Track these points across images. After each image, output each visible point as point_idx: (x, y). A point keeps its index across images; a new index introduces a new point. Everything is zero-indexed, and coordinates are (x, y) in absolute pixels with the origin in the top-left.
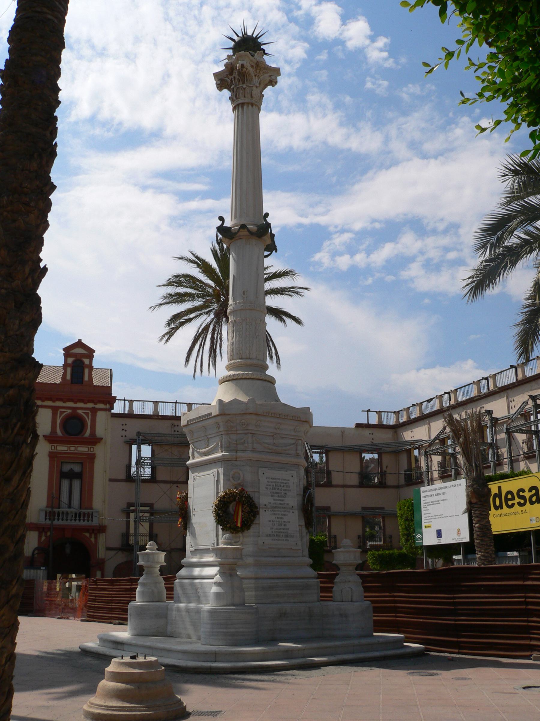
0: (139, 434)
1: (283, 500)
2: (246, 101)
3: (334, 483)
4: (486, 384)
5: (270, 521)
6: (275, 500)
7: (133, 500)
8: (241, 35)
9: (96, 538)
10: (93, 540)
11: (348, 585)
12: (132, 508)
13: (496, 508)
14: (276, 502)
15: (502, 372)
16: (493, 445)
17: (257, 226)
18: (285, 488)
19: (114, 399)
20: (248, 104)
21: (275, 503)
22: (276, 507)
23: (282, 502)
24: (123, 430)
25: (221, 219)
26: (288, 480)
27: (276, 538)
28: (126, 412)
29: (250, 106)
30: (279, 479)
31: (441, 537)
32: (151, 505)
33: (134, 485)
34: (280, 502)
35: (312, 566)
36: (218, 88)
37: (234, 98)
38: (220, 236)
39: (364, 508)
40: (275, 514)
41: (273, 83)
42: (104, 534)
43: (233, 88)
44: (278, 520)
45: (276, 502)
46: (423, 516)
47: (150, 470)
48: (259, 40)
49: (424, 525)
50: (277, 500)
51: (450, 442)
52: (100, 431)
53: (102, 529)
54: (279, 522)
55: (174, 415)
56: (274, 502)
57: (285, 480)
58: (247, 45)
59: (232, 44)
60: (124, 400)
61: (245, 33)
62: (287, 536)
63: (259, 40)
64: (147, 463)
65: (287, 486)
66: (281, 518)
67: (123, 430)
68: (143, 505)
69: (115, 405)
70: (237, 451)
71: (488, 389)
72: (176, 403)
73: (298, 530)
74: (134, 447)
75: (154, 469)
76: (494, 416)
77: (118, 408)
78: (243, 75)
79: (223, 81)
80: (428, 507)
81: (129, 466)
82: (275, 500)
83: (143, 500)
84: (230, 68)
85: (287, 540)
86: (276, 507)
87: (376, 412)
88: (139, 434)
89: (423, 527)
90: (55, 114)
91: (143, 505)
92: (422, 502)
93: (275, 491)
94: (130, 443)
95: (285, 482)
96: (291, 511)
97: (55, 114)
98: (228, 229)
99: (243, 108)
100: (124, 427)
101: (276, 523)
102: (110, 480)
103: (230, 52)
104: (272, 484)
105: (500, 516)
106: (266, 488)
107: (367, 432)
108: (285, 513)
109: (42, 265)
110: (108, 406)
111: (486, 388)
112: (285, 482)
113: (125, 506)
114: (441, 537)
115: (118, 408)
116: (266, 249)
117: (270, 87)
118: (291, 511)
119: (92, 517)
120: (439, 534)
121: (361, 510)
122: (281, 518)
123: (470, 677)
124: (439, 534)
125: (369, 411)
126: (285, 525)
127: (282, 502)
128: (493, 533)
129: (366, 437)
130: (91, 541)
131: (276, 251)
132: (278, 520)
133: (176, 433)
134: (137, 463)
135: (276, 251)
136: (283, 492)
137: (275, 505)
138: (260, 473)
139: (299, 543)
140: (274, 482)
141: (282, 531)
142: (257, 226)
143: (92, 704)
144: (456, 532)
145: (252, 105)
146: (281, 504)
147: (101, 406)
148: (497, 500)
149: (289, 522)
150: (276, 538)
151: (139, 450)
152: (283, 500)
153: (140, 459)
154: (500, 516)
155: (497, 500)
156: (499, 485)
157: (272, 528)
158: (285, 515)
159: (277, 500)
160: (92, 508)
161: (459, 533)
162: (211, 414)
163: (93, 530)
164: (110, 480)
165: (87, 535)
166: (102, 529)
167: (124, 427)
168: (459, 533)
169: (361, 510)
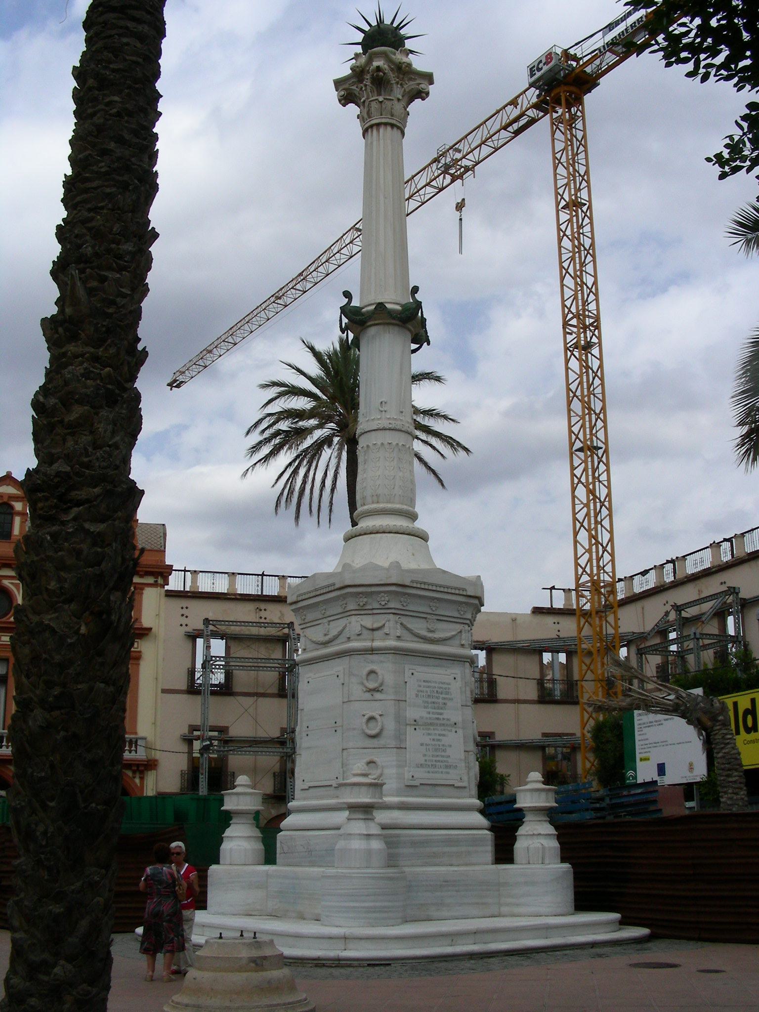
0: (207, 621)
1: (441, 714)
2: (384, 121)
3: (501, 695)
4: (729, 549)
5: (422, 745)
6: (429, 713)
7: (198, 722)
8: (374, 23)
9: (142, 779)
10: (137, 781)
11: (537, 839)
12: (196, 733)
13: (748, 730)
14: (431, 716)
15: (753, 530)
16: (740, 639)
17: (402, 306)
18: (444, 696)
19: (170, 569)
20: (386, 124)
21: (430, 718)
22: (431, 724)
23: (441, 717)
24: (183, 615)
25: (347, 295)
26: (449, 684)
27: (432, 770)
28: (187, 589)
29: (389, 128)
30: (436, 682)
31: (664, 775)
32: (223, 730)
33: (198, 699)
34: (437, 716)
35: (482, 812)
36: (340, 101)
37: (366, 116)
38: (345, 320)
39: (545, 735)
40: (429, 734)
41: (422, 95)
42: (154, 772)
43: (364, 102)
44: (433, 743)
45: (431, 716)
46: (637, 743)
47: (223, 676)
48: (402, 32)
49: (638, 756)
50: (433, 713)
51: (673, 636)
52: (147, 620)
53: (150, 765)
54: (435, 745)
55: (260, 593)
56: (428, 716)
57: (444, 683)
58: (383, 38)
59: (360, 37)
60: (185, 571)
61: (380, 21)
62: (447, 767)
63: (402, 32)
64: (219, 665)
65: (447, 693)
66: (439, 740)
67: (183, 615)
68: (212, 729)
69: (171, 578)
70: (373, 640)
71: (733, 556)
72: (263, 575)
73: (463, 758)
74: (200, 642)
75: (228, 675)
76: (741, 595)
77: (175, 583)
78: (380, 82)
79: (348, 91)
80: (645, 730)
81: (192, 672)
82: (429, 713)
83: (212, 722)
84: (358, 73)
85: (448, 773)
86: (431, 724)
87: (564, 590)
88: (207, 621)
89: (638, 760)
90: (155, 130)
91: (212, 729)
92: (636, 723)
93: (430, 700)
94: (192, 637)
95: (444, 686)
96: (454, 730)
97: (155, 130)
98: (357, 311)
99: (378, 131)
100: (184, 611)
101: (430, 747)
102: (164, 691)
103: (359, 49)
104: (425, 689)
105: (753, 742)
106: (417, 696)
107: (550, 620)
108: (443, 732)
109: (140, 347)
110: (160, 581)
111: (729, 553)
112: (444, 686)
113: (186, 731)
114: (664, 775)
115: (175, 583)
116: (414, 341)
117: (418, 101)
118: (454, 730)
119: (136, 747)
120: (661, 769)
121: (540, 737)
122: (439, 740)
123: (723, 969)
124: (661, 769)
125: (553, 588)
126: (444, 751)
127: (441, 717)
128: (745, 768)
129: (548, 629)
130: (135, 783)
131: (429, 344)
132: (433, 743)
133: (263, 620)
134: (204, 666)
135: (429, 344)
136: (440, 700)
137: (429, 721)
138: (408, 673)
139: (465, 778)
140: (429, 687)
141: (441, 759)
142: (402, 306)
143: (178, 1003)
144: (687, 767)
145: (393, 126)
146: (438, 719)
147: (151, 580)
148: (749, 718)
149: (450, 746)
150: (432, 770)
151: (208, 647)
152: (441, 714)
153: (209, 659)
154: (753, 742)
155: (749, 718)
156: (752, 696)
157: (425, 755)
158: (444, 735)
159: (433, 713)
160: (136, 733)
161: (691, 767)
162: (334, 584)
163: (138, 765)
164: (164, 691)
165: (130, 773)
166: (150, 765)
167: (184, 611)
168: (691, 767)
169: (540, 737)
